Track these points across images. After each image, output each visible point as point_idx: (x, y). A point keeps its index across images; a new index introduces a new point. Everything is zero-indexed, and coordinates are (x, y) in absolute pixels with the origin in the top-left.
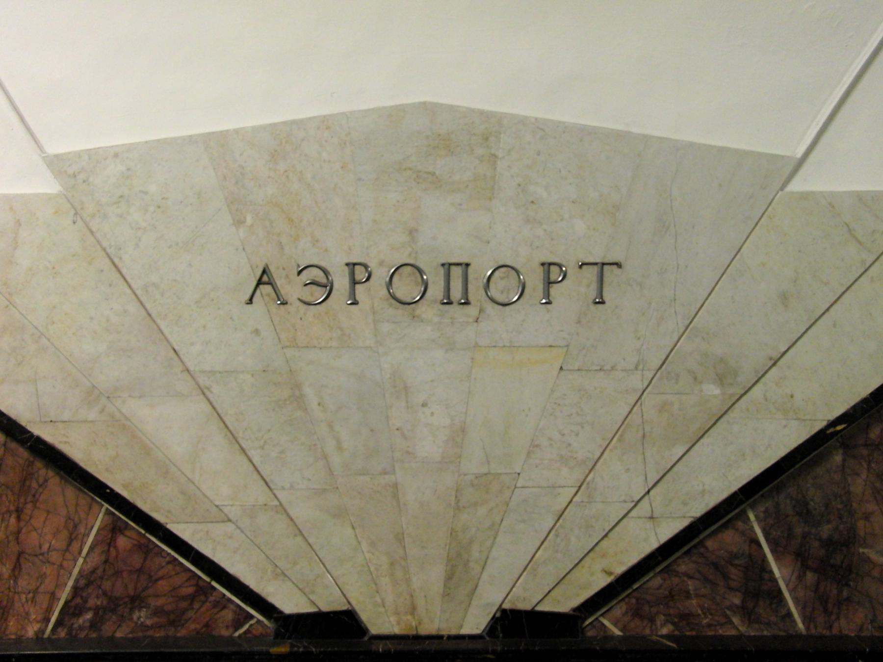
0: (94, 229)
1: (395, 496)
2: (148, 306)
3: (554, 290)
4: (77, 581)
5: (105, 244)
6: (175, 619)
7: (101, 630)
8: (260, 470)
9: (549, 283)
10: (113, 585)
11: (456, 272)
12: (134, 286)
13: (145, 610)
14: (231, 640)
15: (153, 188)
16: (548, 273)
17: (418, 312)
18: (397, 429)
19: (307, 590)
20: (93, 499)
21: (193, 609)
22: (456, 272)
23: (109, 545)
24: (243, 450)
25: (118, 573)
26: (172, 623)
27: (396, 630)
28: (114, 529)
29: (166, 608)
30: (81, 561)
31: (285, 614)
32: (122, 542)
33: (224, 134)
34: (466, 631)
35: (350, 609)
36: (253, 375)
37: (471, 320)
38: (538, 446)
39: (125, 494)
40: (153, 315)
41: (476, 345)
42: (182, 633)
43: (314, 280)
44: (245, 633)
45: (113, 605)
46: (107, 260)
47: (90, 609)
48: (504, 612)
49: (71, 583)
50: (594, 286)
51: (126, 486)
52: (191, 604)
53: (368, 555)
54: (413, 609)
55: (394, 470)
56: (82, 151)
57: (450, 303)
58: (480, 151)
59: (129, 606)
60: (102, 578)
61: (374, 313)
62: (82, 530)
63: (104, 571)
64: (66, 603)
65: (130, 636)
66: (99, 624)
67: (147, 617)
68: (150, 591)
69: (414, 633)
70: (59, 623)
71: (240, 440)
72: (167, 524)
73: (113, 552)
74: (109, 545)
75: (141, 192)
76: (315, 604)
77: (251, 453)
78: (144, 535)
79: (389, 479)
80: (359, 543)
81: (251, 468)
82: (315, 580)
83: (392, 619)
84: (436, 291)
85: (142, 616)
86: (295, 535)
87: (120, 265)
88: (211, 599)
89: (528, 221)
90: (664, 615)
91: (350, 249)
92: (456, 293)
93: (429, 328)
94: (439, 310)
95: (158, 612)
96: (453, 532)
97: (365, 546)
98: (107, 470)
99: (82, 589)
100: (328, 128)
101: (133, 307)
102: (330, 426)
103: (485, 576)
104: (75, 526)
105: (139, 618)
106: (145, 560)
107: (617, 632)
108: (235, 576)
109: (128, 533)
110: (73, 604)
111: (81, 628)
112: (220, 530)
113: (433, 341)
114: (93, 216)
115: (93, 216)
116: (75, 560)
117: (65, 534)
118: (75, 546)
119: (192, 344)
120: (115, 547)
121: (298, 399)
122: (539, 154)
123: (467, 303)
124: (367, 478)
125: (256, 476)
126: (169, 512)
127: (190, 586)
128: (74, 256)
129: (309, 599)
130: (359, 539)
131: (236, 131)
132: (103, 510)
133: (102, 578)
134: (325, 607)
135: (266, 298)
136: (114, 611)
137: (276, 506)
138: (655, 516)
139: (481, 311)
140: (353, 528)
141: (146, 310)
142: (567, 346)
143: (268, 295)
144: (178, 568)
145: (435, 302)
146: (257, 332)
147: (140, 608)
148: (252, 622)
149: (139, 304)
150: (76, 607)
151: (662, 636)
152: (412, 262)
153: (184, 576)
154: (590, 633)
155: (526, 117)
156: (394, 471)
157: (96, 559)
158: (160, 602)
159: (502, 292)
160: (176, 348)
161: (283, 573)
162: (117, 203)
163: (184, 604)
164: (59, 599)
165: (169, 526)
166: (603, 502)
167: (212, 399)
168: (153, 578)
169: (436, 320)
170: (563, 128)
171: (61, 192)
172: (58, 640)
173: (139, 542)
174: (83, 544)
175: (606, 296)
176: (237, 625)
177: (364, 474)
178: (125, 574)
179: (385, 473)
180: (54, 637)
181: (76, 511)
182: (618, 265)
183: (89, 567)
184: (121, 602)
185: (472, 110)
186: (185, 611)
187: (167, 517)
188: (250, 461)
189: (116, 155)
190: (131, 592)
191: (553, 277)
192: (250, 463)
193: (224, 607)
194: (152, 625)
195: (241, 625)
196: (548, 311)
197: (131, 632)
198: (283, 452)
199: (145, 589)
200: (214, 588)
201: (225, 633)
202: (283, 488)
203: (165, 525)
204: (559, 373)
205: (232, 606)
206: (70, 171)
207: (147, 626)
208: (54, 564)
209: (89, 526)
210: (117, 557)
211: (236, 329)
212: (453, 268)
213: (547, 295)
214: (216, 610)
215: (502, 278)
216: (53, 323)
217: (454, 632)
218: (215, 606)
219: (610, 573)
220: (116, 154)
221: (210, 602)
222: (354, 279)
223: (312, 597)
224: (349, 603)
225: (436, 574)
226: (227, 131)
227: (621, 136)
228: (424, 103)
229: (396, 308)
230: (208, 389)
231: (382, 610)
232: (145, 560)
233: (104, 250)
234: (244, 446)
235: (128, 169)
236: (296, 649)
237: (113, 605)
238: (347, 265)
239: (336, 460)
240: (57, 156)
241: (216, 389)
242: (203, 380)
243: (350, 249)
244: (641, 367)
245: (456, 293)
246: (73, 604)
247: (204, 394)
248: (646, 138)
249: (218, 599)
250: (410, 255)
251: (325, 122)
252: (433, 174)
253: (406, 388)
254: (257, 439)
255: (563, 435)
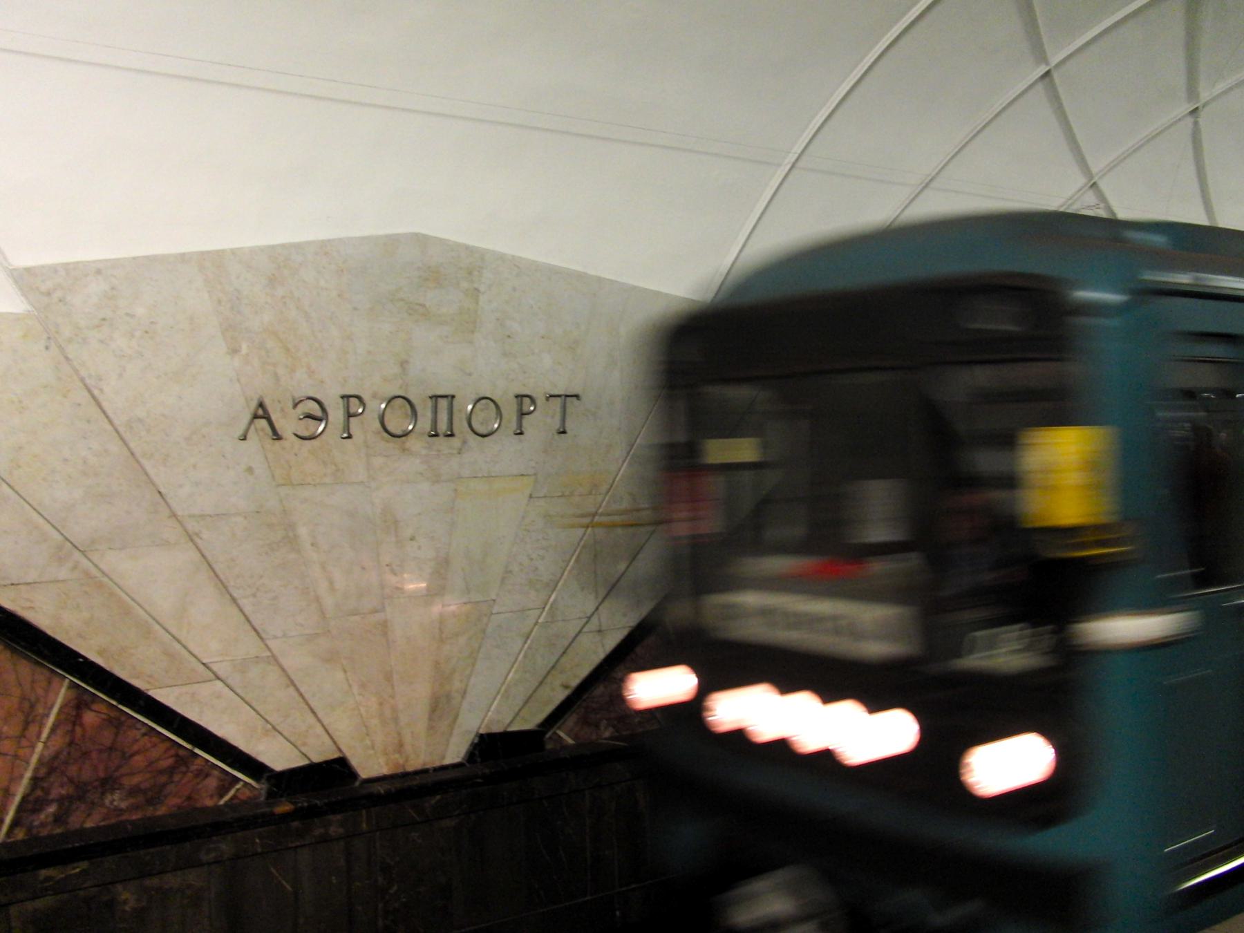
0: (70, 356)
1: (385, 634)
2: (132, 445)
3: (527, 420)
4: (36, 770)
5: (83, 373)
6: (154, 796)
7: (67, 823)
8: (251, 619)
9: (522, 414)
10: (80, 769)
11: (443, 403)
12: (116, 422)
13: (118, 791)
14: (217, 809)
15: (140, 311)
16: (521, 405)
17: (408, 445)
18: (387, 565)
19: (299, 743)
20: (53, 671)
21: (172, 782)
22: (443, 403)
23: (74, 724)
24: (234, 600)
25: (86, 754)
26: (151, 802)
27: (385, 771)
28: (80, 704)
29: (143, 786)
30: (40, 746)
31: (277, 772)
32: (89, 718)
33: (219, 254)
34: (448, 761)
35: (341, 756)
36: (245, 518)
37: (455, 452)
38: (511, 572)
39: (99, 661)
40: (138, 455)
41: (460, 477)
42: (162, 811)
43: (309, 413)
44: (232, 799)
45: (81, 792)
46: (86, 393)
47: (52, 801)
48: (481, 737)
49: (28, 775)
50: (558, 417)
51: (101, 653)
52: (171, 776)
53: (358, 698)
54: (400, 746)
55: (384, 607)
56: (58, 265)
57: (436, 435)
58: (465, 285)
59: (100, 790)
60: (66, 763)
61: (367, 447)
62: (40, 710)
63: (69, 753)
64: (24, 799)
65: (102, 824)
66: (65, 816)
67: (121, 800)
68: (123, 770)
69: (401, 770)
70: (16, 823)
71: (231, 589)
72: (148, 690)
73: (78, 730)
74: (74, 724)
75: (127, 314)
76: (306, 756)
77: (242, 602)
78: (117, 707)
79: (379, 617)
80: (350, 686)
81: (242, 618)
82: (307, 731)
83: (380, 760)
84: (425, 423)
85: (116, 799)
86: (288, 686)
87: (101, 398)
88: (193, 768)
89: (505, 354)
90: (607, 720)
91: (345, 381)
92: (443, 426)
93: (418, 461)
94: (428, 443)
95: (134, 791)
96: (437, 664)
97: (355, 690)
98: (80, 636)
99: (42, 779)
100: (326, 254)
101: (115, 447)
102: (323, 568)
103: (465, 705)
104: (32, 707)
105: (112, 802)
106: (116, 735)
107: (570, 741)
108: (224, 738)
109: (95, 707)
110: (31, 798)
111: (43, 825)
112: (205, 690)
113: (421, 474)
114: (70, 341)
115: (70, 341)
116: (33, 747)
117: (20, 717)
118: (33, 729)
119: (181, 486)
120: (82, 725)
121: (291, 541)
122: (514, 289)
123: (452, 435)
124: (357, 618)
125: (247, 627)
126: (151, 676)
127: (168, 758)
128: (46, 387)
129: (301, 752)
130: (351, 682)
131: (233, 252)
132: (67, 681)
133: (66, 763)
134: (317, 758)
135: (261, 433)
136: (81, 798)
137: (268, 657)
138: (603, 628)
139: (465, 442)
140: (345, 672)
141: (129, 449)
142: (535, 474)
143: (263, 430)
144: (154, 739)
145: (423, 434)
146: (250, 470)
147: (113, 790)
148: (238, 786)
149: (120, 443)
150: (37, 800)
151: (606, 739)
152: (403, 394)
153: (162, 747)
154: (549, 746)
155: (505, 254)
156: (383, 609)
157: (59, 741)
158: (136, 780)
159: (482, 424)
160: (162, 490)
161: (274, 728)
162: (98, 326)
163: (163, 779)
164: (14, 795)
165: (150, 693)
166: (563, 620)
167: (201, 547)
168: (127, 755)
169: (424, 452)
170: (535, 267)
171: (29, 311)
172: (15, 843)
173: (109, 715)
174: (42, 726)
175: (569, 426)
176: (222, 791)
177: (356, 615)
178: (94, 755)
179: (375, 611)
180: (9, 840)
181: (33, 688)
182: (577, 396)
183: (46, 753)
184: (89, 788)
185: (458, 245)
186: (164, 785)
187: (149, 683)
188: (241, 610)
189: (99, 272)
190: (102, 775)
191: (525, 409)
192: (240, 613)
193: (207, 775)
194: (127, 808)
195: (227, 790)
196: (520, 441)
197: (104, 820)
198: (275, 598)
199: (119, 767)
200: (197, 755)
201: (209, 803)
202: (275, 637)
203: (146, 692)
204: (529, 501)
205: (216, 773)
206: (43, 288)
207: (121, 810)
208: (6, 755)
209: (49, 704)
210: (83, 736)
211: (228, 468)
212: (440, 400)
213: (520, 425)
214: (198, 780)
215: (482, 410)
216: (19, 467)
217: (437, 764)
218: (197, 776)
219: (566, 687)
220: (99, 270)
221: (192, 772)
222: (348, 412)
223: (304, 749)
224: (340, 750)
225: (421, 709)
226: (223, 251)
227: (582, 277)
228: (416, 234)
229: (388, 441)
230: (197, 534)
231: (372, 752)
232: (116, 735)
233: (82, 380)
234: (235, 595)
235: (113, 288)
236: (300, 805)
237: (81, 792)
238: (343, 397)
239: (329, 602)
240: (28, 270)
241: (206, 534)
242: (192, 526)
243: (345, 381)
244: (594, 492)
245: (443, 426)
246: (31, 798)
247: (192, 540)
248: (600, 280)
249: (200, 767)
250: (401, 387)
251: (324, 248)
252: (423, 306)
253: (396, 522)
254: (249, 586)
255: (532, 559)
